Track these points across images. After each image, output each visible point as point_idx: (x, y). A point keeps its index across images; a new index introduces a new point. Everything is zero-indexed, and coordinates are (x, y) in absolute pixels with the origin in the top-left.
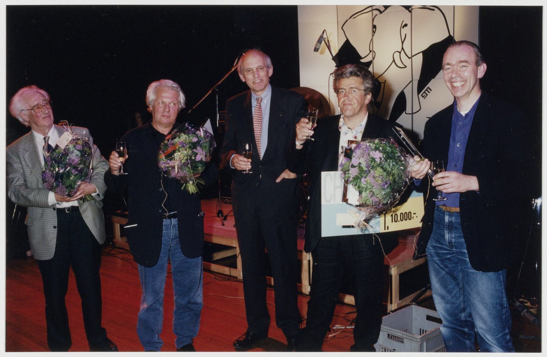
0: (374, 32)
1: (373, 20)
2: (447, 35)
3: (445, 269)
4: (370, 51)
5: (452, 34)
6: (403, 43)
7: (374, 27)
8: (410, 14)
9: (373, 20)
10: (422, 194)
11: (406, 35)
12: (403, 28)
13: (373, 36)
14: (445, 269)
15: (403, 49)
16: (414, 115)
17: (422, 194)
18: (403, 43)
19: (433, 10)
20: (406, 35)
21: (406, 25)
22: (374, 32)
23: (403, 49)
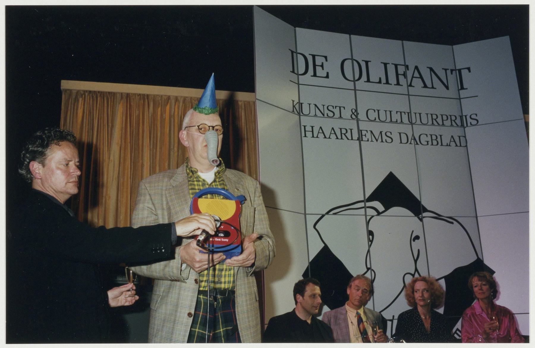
0: (371, 241)
1: (368, 223)
2: (476, 258)
3: (199, 269)
4: (368, 269)
5: (480, 257)
6: (416, 261)
7: (371, 233)
8: (421, 223)
9: (368, 223)
10: (506, 40)
11: (419, 250)
12: (414, 241)
13: (370, 246)
14: (199, 269)
15: (416, 270)
16: (410, 94)
17: (506, 40)
18: (416, 261)
19: (452, 223)
20: (419, 250)
21: (417, 238)
22: (372, 241)
23: (416, 270)
